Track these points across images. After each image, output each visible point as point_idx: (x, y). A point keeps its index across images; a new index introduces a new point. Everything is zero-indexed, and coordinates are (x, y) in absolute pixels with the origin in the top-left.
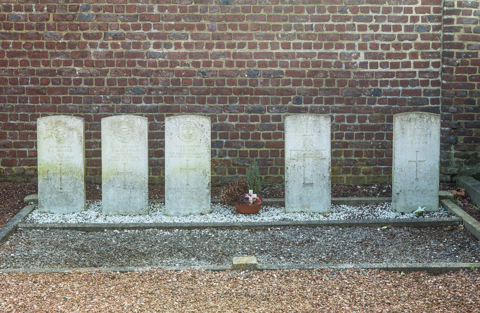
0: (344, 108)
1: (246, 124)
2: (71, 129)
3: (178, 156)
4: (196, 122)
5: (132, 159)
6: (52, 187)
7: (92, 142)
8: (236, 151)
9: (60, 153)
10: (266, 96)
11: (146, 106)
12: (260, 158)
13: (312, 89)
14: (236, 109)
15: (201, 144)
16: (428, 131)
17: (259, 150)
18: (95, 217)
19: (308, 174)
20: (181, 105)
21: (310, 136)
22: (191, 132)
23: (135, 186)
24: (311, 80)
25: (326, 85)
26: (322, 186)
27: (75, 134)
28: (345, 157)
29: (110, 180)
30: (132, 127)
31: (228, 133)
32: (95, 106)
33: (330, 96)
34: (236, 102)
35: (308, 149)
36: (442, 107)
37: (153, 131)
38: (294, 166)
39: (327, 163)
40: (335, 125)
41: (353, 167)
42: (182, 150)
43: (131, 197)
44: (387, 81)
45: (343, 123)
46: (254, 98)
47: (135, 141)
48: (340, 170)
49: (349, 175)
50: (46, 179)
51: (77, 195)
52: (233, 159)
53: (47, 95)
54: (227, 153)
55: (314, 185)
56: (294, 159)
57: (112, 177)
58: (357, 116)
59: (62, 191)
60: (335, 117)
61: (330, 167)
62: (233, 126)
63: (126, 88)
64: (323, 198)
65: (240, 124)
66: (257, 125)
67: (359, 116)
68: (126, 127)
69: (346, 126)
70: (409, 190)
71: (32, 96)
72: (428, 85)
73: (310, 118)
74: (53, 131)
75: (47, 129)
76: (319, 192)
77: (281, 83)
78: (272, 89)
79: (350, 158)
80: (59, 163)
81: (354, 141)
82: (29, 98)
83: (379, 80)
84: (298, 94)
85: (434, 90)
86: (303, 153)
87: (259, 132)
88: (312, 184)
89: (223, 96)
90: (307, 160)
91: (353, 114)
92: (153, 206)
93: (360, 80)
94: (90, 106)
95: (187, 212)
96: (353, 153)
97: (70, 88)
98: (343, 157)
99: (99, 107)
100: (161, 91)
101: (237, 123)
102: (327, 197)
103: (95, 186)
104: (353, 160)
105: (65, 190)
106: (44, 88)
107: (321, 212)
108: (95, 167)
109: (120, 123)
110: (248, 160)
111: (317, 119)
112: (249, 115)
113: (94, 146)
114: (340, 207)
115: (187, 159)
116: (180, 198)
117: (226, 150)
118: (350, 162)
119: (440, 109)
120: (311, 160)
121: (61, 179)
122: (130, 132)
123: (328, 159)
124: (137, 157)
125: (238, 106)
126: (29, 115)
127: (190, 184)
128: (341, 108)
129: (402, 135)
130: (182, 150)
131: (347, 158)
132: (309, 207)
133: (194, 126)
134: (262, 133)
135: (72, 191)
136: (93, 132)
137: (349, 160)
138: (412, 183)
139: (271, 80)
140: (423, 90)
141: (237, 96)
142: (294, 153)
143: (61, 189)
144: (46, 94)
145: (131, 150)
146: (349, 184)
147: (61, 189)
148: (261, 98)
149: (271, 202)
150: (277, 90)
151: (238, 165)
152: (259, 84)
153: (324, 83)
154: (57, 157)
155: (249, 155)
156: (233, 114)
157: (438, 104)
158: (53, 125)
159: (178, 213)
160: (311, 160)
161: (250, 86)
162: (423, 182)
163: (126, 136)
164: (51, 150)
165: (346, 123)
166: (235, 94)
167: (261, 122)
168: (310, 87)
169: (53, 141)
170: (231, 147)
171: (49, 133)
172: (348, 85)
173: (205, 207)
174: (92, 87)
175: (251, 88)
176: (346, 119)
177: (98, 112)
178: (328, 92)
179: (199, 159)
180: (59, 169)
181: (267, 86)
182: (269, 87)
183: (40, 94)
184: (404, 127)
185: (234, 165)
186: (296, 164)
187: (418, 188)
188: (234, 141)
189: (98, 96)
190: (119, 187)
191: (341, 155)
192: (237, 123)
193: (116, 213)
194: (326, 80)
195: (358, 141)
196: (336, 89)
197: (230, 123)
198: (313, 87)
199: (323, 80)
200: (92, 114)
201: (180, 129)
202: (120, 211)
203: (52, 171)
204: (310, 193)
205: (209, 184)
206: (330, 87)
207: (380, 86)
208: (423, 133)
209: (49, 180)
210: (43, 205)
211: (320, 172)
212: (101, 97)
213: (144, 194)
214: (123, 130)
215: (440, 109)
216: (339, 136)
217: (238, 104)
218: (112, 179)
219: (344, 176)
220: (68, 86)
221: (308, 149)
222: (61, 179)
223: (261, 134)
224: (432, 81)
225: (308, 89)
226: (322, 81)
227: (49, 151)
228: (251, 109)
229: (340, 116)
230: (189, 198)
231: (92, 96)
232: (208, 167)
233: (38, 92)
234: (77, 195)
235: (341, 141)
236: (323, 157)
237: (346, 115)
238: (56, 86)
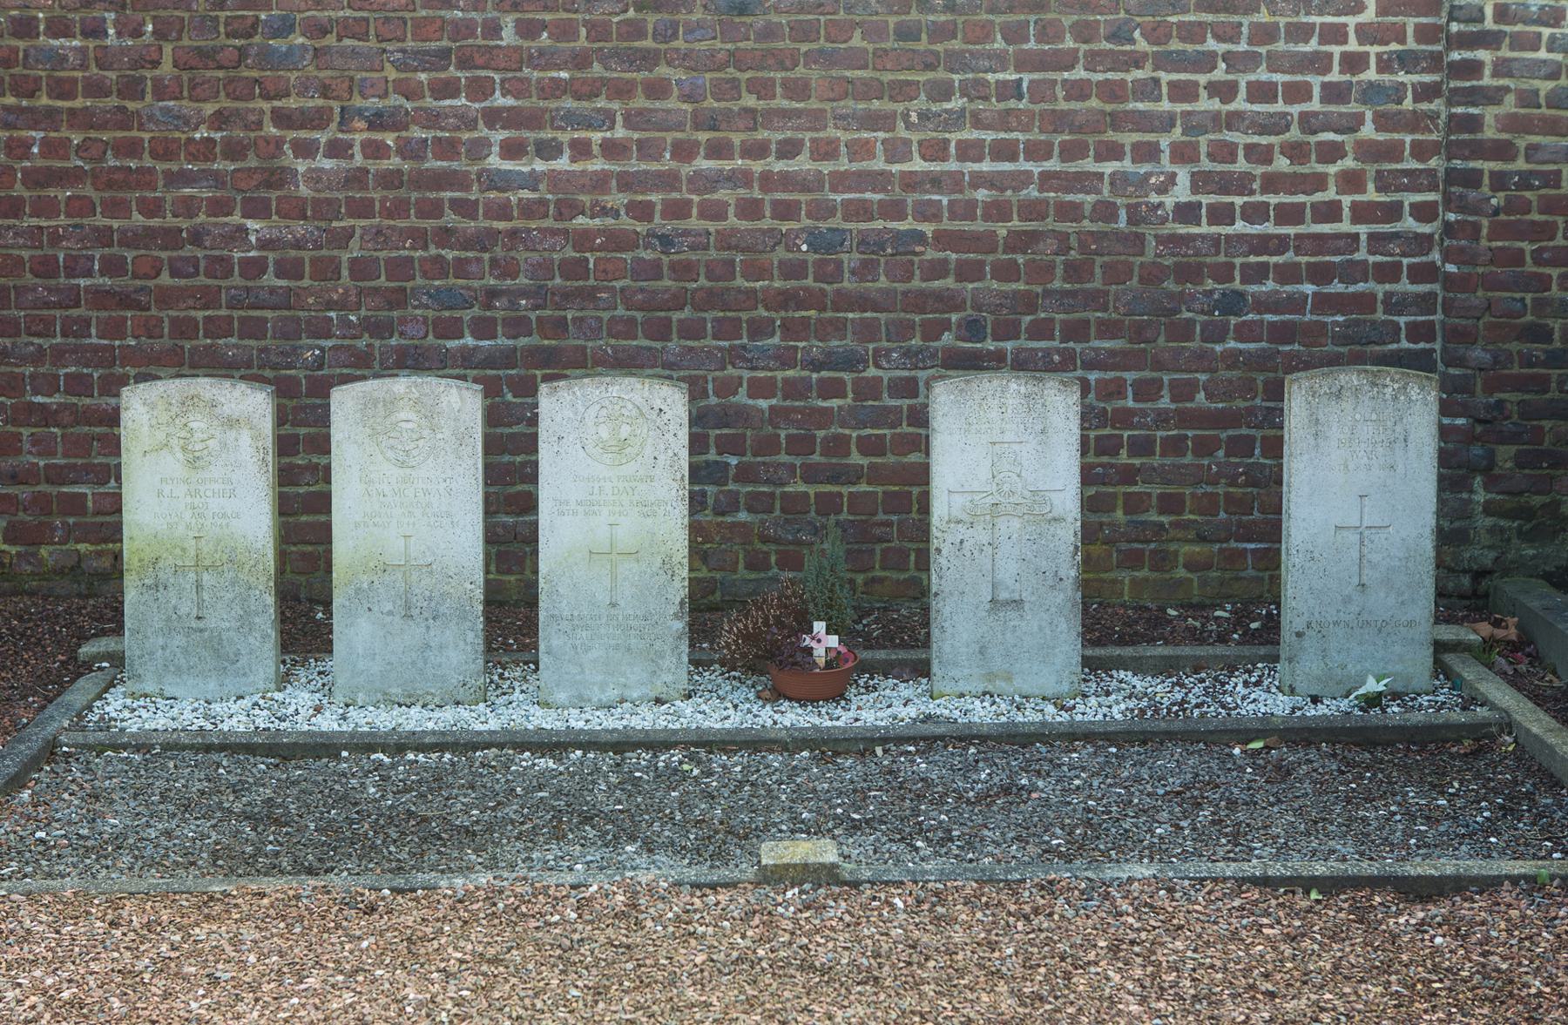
2: (231, 423)
3: (580, 509)
4: (638, 400)
5: (432, 519)
6: (171, 612)
7: (299, 466)
8: (772, 495)
9: (197, 501)
11: (476, 348)
14: (769, 357)
15: (658, 471)
16: (1398, 428)
17: (845, 490)
18: (311, 711)
19: (1008, 569)
20: (590, 344)
22: (625, 431)
23: (442, 609)
25: (1065, 280)
26: (1053, 609)
27: (245, 438)
28: (1125, 513)
29: (358, 590)
30: (430, 415)
31: (744, 435)
32: (311, 348)
33: (1077, 315)
34: (772, 335)
36: (1444, 349)
37: (499, 430)
39: (1067, 534)
41: (1152, 546)
42: (596, 491)
43: (428, 646)
44: (1265, 265)
45: (1120, 403)
46: (830, 321)
47: (441, 460)
50: (149, 587)
51: (251, 640)
52: (763, 522)
53: (154, 312)
54: (742, 501)
56: (959, 522)
57: (364, 581)
58: (1166, 378)
59: (201, 625)
61: (1076, 547)
62: (763, 412)
63: (412, 289)
65: (782, 408)
67: (1171, 381)
68: (412, 416)
70: (1336, 623)
71: (105, 314)
72: (1397, 280)
73: (1013, 386)
74: (171, 430)
75: (154, 422)
76: (1041, 628)
77: (917, 272)
78: (886, 292)
79: (1143, 517)
80: (191, 534)
81: (1156, 461)
82: (94, 322)
83: (1238, 261)
84: (972, 308)
85: (1418, 295)
86: (990, 500)
87: (847, 432)
88: (1018, 603)
89: (729, 314)
90: (1002, 524)
91: (1155, 374)
92: (501, 676)
93: (1175, 264)
94: (295, 349)
95: (612, 694)
96: (1154, 501)
97: (228, 289)
98: (1119, 514)
99: (322, 349)
100: (527, 299)
101: (774, 401)
102: (1067, 645)
103: (311, 610)
104: (1155, 524)
105: (211, 622)
106: (142, 289)
108: (310, 548)
109: (391, 403)
110: (810, 523)
112: (815, 376)
113: (308, 477)
115: (612, 520)
116: (588, 650)
117: (738, 493)
119: (1438, 356)
121: (199, 586)
122: (426, 433)
123: (1070, 519)
124: (449, 515)
125: (778, 347)
126: (96, 375)
127: (622, 603)
128: (1112, 353)
129: (1313, 442)
130: (596, 491)
131: (1135, 518)
132: (1009, 678)
133: (635, 412)
135: (234, 624)
136: (303, 431)
137: (1143, 523)
138: (1347, 600)
139: (886, 263)
140: (1380, 296)
141: (773, 314)
142: (958, 500)
143: (199, 618)
144: (149, 309)
145: (427, 492)
147: (199, 618)
148: (853, 320)
150: (905, 294)
151: (777, 541)
152: (847, 275)
153: (1059, 271)
154: (188, 515)
155: (813, 508)
156: (761, 374)
157: (1432, 339)
158: (174, 410)
159: (581, 697)
162: (1382, 595)
163: (413, 445)
164: (167, 491)
165: (1130, 403)
166: (767, 309)
167: (854, 400)
168: (1014, 286)
169: (172, 463)
170: (755, 481)
171: (160, 436)
172: (1135, 279)
173: (669, 678)
174: (299, 283)
175: (821, 289)
177: (320, 367)
179: (649, 521)
180: (193, 553)
181: (873, 281)
183: (129, 307)
184: (1321, 416)
185: (765, 540)
186: (966, 537)
187: (1365, 616)
188: (764, 463)
189: (321, 314)
190: (390, 613)
191: (1113, 509)
192: (774, 401)
193: (379, 696)
195: (1168, 461)
196: (1098, 291)
197: (751, 402)
200: (301, 374)
201: (590, 422)
202: (393, 690)
203: (171, 561)
205: (682, 603)
206: (1077, 286)
207: (1242, 282)
208: (1382, 437)
209: (161, 589)
210: (140, 671)
212: (331, 319)
213: (470, 635)
214: (403, 425)
215: (1438, 356)
217: (776, 340)
218: (365, 586)
219: (1125, 576)
220: (223, 283)
221: (1006, 488)
222: (199, 586)
224: (1409, 266)
225: (1006, 292)
227: (160, 493)
229: (1111, 380)
230: (617, 648)
231: (301, 313)
232: (678, 545)
233: (125, 300)
234: (251, 640)
236: (1055, 514)
237: (1130, 376)
238: (183, 282)
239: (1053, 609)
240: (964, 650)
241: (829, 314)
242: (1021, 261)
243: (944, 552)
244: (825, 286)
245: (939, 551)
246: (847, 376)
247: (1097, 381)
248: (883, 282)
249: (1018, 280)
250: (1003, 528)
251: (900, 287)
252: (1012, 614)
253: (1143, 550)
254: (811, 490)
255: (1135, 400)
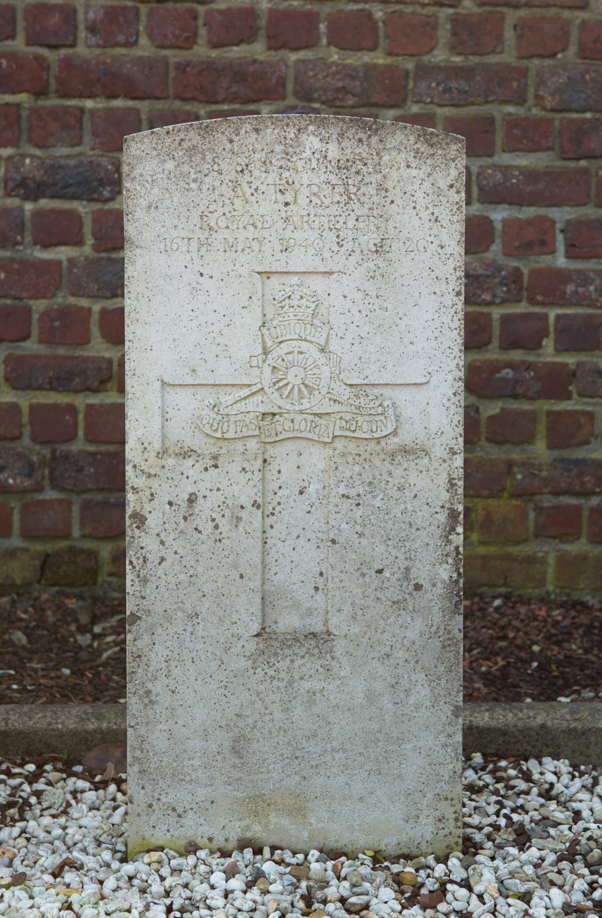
0: (552, 176)
1: (12, 260)
10: (119, 103)
12: (91, 448)
13: (375, 67)
17: (81, 401)
19: (297, 564)
21: (310, 281)
24: (369, 16)
25: (453, 49)
26: (400, 655)
28: (551, 446)
33: (472, 110)
35: (294, 377)
38: (192, 500)
39: (434, 482)
40: (500, 269)
45: (544, 261)
46: (55, 113)
48: (525, 517)
49: (572, 548)
55: (340, 647)
56: (186, 453)
60: (499, 226)
61: (453, 515)
64: (400, 741)
66: (72, 261)
69: (561, 276)
73: (312, 142)
76: (371, 697)
77: (203, 32)
78: (147, 64)
79: (580, 453)
84: (296, 94)
86: (256, 406)
87: (84, 302)
88: (318, 640)
90: (285, 459)
98: (540, 448)
102: (428, 715)
107: (389, 843)
110: (20, 456)
111: (363, 150)
112: (29, 206)
114: (527, 777)
118: (581, 475)
120: (316, 459)
123: (439, 451)
128: (532, 175)
131: (567, 454)
132: (298, 809)
134: (96, 308)
137: (578, 462)
139: (150, 15)
142: (185, 405)
146: (575, 596)
148: (93, 112)
149: (74, 733)
150: (181, 68)
152: (82, 34)
153: (444, 34)
155: (27, 431)
160: (316, 459)
161: (29, 43)
165: (561, 261)
167: (96, 248)
168: (367, 58)
172: (573, 49)
175: (37, 57)
176: (560, 237)
178: (464, 85)
181: (127, 45)
182: (137, 52)
186: (202, 489)
191: (530, 439)
194: (455, 20)
196: (509, 68)
198: (379, 59)
199: (435, 16)
204: (311, 703)
206: (474, 60)
211: (378, 552)
216: (522, 335)
219: (549, 552)
221: (294, 377)
223: (95, 317)
225: (354, 69)
226: (430, 25)
228: (38, 175)
229: (529, 222)
235: (531, 358)
236: (405, 438)
237: (561, 215)
239: (400, 655)
240: (196, 744)
241: (53, 102)
242: (379, 15)
243: (152, 521)
244: (44, 52)
245: (140, 519)
246: (82, 208)
247: (505, 222)
248: (145, 48)
249: (373, 48)
250: (288, 469)
251: (174, 56)
252: (307, 665)
253: (578, 509)
254: (25, 401)
255: (569, 256)
